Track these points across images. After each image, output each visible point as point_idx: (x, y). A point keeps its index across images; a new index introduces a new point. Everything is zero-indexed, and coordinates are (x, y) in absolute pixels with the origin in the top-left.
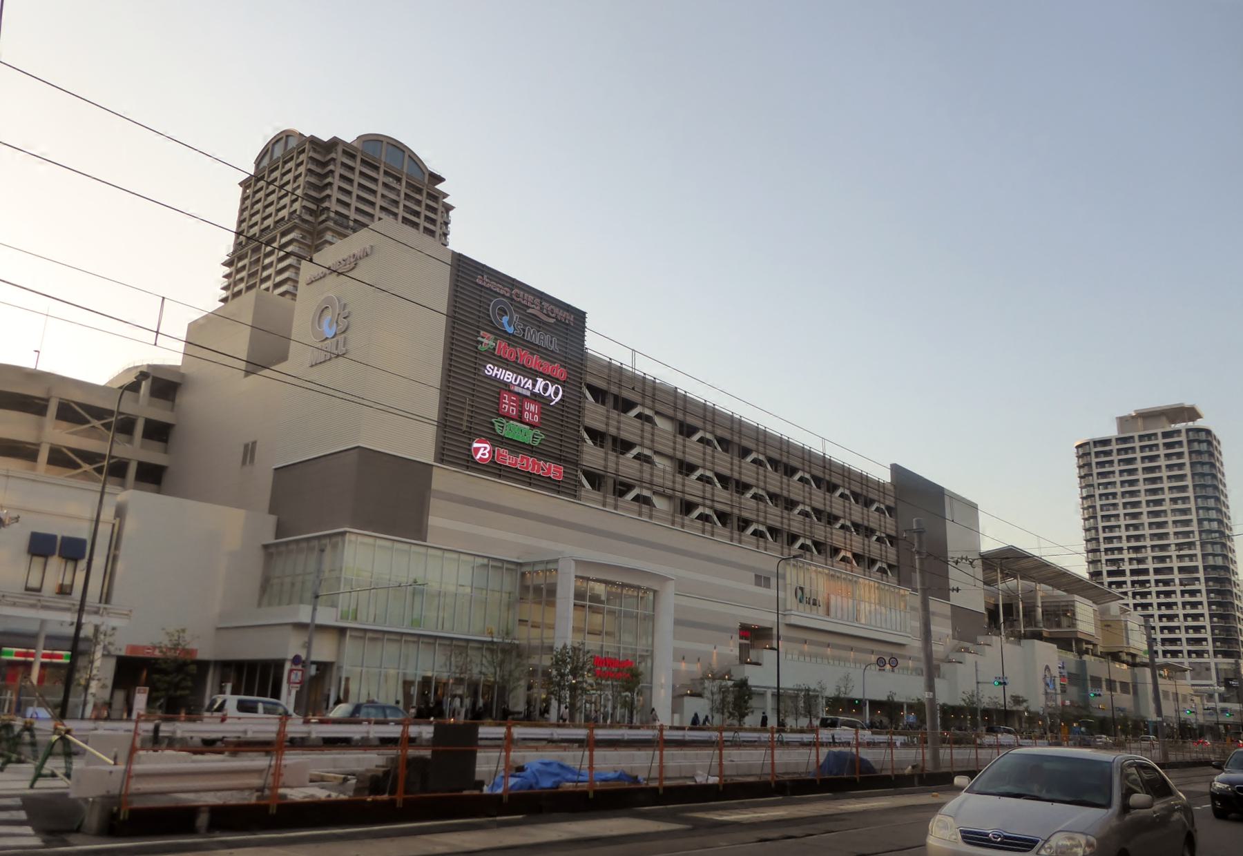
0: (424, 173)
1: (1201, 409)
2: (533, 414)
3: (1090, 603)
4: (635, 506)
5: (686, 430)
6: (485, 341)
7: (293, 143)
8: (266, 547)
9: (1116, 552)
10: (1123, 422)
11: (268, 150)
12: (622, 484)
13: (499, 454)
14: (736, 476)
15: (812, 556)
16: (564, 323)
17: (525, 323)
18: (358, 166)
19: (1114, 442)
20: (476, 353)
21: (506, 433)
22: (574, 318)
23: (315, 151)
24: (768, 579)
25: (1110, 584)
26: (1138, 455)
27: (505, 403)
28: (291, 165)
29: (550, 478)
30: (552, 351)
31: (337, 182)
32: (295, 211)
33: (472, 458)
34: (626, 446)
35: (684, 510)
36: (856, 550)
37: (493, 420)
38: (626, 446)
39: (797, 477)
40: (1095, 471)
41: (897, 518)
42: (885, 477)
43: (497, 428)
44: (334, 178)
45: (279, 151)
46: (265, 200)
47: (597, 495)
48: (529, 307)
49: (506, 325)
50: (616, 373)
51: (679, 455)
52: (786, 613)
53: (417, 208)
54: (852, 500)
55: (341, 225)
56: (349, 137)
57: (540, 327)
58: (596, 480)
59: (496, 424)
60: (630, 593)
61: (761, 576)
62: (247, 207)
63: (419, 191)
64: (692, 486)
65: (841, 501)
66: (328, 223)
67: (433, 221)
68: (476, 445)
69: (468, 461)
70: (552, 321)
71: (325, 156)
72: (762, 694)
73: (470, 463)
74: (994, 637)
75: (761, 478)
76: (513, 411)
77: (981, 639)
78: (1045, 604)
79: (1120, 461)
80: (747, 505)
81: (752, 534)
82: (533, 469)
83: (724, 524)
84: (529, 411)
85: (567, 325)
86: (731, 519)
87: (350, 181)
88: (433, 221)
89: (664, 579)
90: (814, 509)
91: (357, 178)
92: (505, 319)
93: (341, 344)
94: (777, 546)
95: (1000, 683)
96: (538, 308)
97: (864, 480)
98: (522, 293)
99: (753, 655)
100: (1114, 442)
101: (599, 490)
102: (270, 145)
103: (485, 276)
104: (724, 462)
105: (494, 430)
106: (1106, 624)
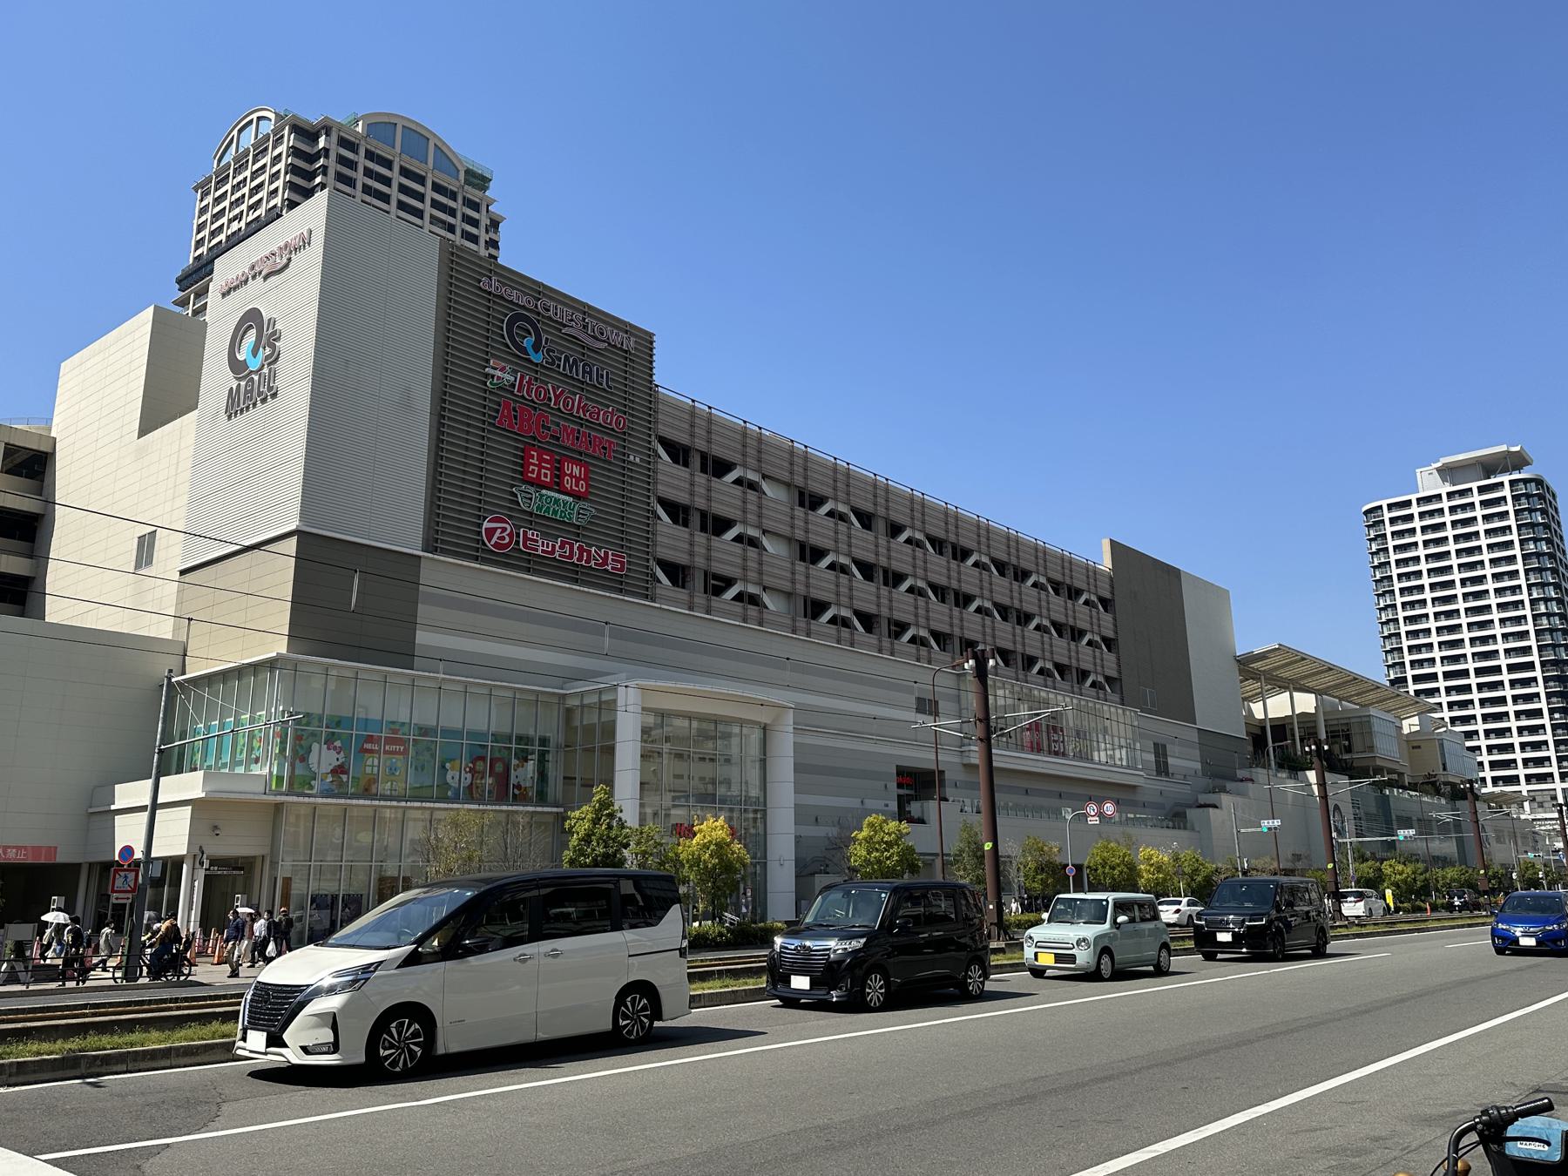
0: (458, 171)
1: (1531, 454)
2: (578, 480)
4: (738, 607)
9: (1423, 649)
12: (716, 577)
15: (1054, 682)
16: (621, 349)
25: (1417, 693)
26: (1448, 518)
27: (533, 464)
28: (267, 160)
29: (606, 570)
34: (720, 525)
36: (1059, 659)
38: (720, 525)
40: (1391, 543)
41: (1115, 613)
48: (565, 326)
49: (530, 350)
52: (964, 749)
53: (450, 220)
54: (1100, 607)
58: (678, 574)
61: (925, 700)
63: (453, 196)
64: (820, 582)
65: (1086, 609)
69: (477, 550)
72: (931, 864)
74: (1260, 770)
77: (1241, 773)
80: (900, 603)
81: (1091, 686)
82: (580, 559)
84: (571, 475)
85: (626, 352)
86: (1070, 670)
99: (915, 808)
101: (683, 587)
102: (235, 132)
104: (865, 544)
105: (519, 504)
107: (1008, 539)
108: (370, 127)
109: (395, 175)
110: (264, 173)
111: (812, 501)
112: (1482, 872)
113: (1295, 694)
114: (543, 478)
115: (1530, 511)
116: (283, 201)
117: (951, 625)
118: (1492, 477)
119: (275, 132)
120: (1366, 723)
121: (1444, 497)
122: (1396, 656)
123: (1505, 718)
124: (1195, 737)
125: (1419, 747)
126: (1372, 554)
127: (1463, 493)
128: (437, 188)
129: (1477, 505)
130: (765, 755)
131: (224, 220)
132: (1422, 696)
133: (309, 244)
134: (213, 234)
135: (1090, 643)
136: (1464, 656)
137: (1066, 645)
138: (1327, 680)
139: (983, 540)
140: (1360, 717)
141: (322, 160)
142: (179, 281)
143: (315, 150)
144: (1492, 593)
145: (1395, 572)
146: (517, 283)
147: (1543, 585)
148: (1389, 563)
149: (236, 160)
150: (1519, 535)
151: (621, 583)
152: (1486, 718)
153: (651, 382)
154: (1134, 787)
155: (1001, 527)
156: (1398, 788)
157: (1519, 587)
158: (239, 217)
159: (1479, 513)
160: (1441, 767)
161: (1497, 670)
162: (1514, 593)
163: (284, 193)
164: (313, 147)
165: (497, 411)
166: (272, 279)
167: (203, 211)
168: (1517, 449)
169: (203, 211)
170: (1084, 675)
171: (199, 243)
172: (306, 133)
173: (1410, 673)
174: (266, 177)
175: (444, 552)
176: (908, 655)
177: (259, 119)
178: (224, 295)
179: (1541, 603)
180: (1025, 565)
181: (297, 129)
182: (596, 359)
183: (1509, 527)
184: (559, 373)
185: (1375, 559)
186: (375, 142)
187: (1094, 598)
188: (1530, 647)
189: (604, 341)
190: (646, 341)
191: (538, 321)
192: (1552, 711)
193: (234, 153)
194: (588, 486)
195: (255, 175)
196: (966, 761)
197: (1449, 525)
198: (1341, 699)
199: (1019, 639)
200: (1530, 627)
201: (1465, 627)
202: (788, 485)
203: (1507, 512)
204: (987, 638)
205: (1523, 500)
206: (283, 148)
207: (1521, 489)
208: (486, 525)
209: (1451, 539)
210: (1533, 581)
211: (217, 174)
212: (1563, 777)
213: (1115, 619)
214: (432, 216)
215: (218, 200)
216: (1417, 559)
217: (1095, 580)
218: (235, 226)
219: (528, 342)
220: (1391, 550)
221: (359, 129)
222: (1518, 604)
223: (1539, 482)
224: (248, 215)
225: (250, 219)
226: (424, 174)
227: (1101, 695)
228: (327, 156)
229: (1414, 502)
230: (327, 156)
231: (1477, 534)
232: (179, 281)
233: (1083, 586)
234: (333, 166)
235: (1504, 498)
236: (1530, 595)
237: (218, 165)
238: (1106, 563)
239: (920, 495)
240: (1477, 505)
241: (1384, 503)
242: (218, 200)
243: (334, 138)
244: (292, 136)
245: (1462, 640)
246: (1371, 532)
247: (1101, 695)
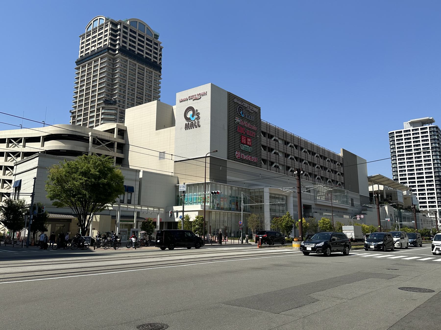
0: (152, 34)
1: (435, 119)
5: (286, 143)
6: (237, 120)
14: (268, 146)
15: (321, 181)
18: (129, 32)
25: (401, 183)
26: (412, 136)
28: (103, 31)
36: (310, 172)
39: (273, 139)
40: (396, 142)
48: (247, 108)
49: (242, 114)
50: (268, 126)
51: (285, 152)
52: (315, 200)
53: (151, 48)
58: (265, 161)
63: (151, 42)
67: (156, 54)
69: (235, 158)
78: (387, 193)
81: (290, 171)
82: (250, 160)
85: (256, 112)
86: (335, 181)
88: (156, 54)
90: (309, 162)
91: (129, 37)
97: (334, 155)
102: (92, 22)
104: (296, 152)
105: (240, 148)
107: (284, 133)
108: (130, 22)
109: (137, 36)
110: (102, 34)
111: (286, 143)
112: (416, 230)
113: (380, 185)
115: (434, 135)
116: (109, 43)
117: (267, 157)
118: (424, 125)
119: (105, 23)
120: (396, 193)
121: (411, 130)
122: (396, 173)
123: (424, 190)
124: (359, 197)
125: (406, 199)
126: (391, 145)
127: (416, 130)
128: (147, 39)
129: (420, 133)
130: (287, 202)
131: (90, 46)
132: (411, 187)
133: (206, 95)
134: (86, 50)
135: (305, 163)
136: (414, 173)
137: (298, 163)
138: (386, 183)
139: (277, 133)
140: (395, 192)
141: (119, 32)
142: (76, 62)
143: (117, 29)
144: (422, 157)
145: (397, 150)
146: (239, 99)
147: (436, 155)
148: (395, 148)
149: (93, 30)
150: (431, 142)
151: (256, 164)
152: (419, 190)
153: (260, 119)
154: (347, 209)
155: (273, 126)
156: (402, 209)
157: (430, 156)
158: (95, 46)
159: (420, 135)
160: (412, 204)
161: (423, 177)
162: (428, 157)
163: (109, 41)
164: (116, 28)
165: (237, 128)
166: (195, 101)
167: (83, 43)
168: (431, 118)
169: (83, 43)
170: (272, 163)
171: (82, 52)
172: (115, 24)
173: (399, 177)
174: (103, 35)
175: (251, 165)
176: (273, 170)
177: (100, 19)
178: (180, 102)
179: (436, 160)
180: (271, 133)
181: (112, 23)
182: (252, 115)
183: (428, 139)
184: (246, 119)
185: (391, 147)
186: (132, 27)
187: (306, 150)
188: (432, 172)
190: (259, 109)
192: (437, 189)
193: (92, 28)
194: (251, 143)
195: (99, 35)
196: (316, 203)
197: (412, 138)
198: (389, 187)
199: (285, 161)
200: (432, 166)
201: (415, 166)
202: (282, 140)
203: (428, 135)
204: (277, 161)
205: (432, 132)
206: (108, 28)
207: (432, 129)
208: (236, 153)
209: (412, 142)
210: (434, 154)
211: (87, 33)
212: (439, 206)
213: (343, 169)
214: (146, 47)
215: (87, 41)
216: (403, 147)
217: (293, 139)
218: (93, 48)
219: (241, 112)
220: (396, 144)
221: (128, 23)
222: (429, 160)
223: (437, 128)
224: (97, 46)
225: (98, 47)
226: (144, 35)
227: (320, 181)
228: (120, 31)
229: (403, 132)
230: (120, 31)
231: (419, 141)
232: (76, 62)
233: (290, 141)
234: (122, 34)
235: (427, 132)
236: (433, 158)
237: (87, 31)
238: (341, 154)
239: (269, 124)
240: (420, 133)
241: (395, 131)
242: (87, 41)
243: (122, 26)
244: (111, 25)
245: (414, 169)
246: (391, 139)
247: (320, 181)
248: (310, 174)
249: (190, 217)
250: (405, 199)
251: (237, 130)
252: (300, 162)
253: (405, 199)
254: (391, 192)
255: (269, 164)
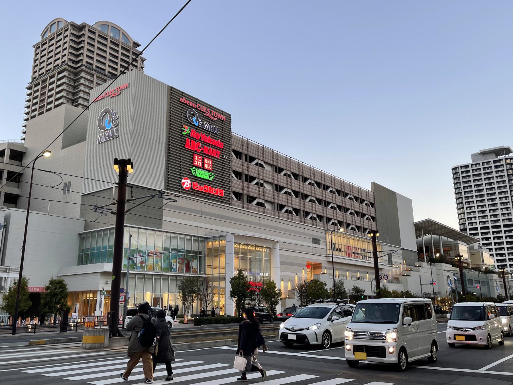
0: (130, 42)
2: (209, 165)
3: (465, 244)
7: (62, 25)
8: (80, 234)
10: (473, 156)
11: (48, 29)
12: (251, 197)
13: (194, 185)
15: (356, 233)
17: (203, 121)
18: (97, 38)
19: (470, 166)
20: (181, 136)
21: (198, 175)
22: (226, 118)
23: (74, 29)
24: (318, 240)
25: (471, 234)
26: (482, 172)
28: (61, 37)
30: (216, 134)
31: (86, 46)
32: (65, 61)
33: (182, 187)
34: (251, 179)
35: (279, 209)
37: (191, 169)
38: (251, 179)
40: (462, 180)
41: (375, 208)
42: (368, 187)
43: (193, 172)
44: (84, 44)
45: (54, 30)
46: (41, 53)
47: (240, 203)
48: (205, 113)
49: (195, 122)
52: (328, 256)
55: (89, 68)
56: (91, 22)
57: (210, 122)
58: (239, 196)
59: (192, 170)
60: (259, 249)
62: (38, 59)
63: (128, 51)
64: (282, 198)
66: (82, 67)
68: (183, 181)
69: (180, 189)
70: (216, 119)
71: (79, 33)
73: (181, 189)
75: (289, 183)
76: (200, 164)
79: (473, 175)
82: (210, 192)
83: (297, 214)
84: (207, 164)
85: (222, 121)
87: (93, 46)
89: (275, 242)
91: (96, 45)
92: (194, 119)
93: (115, 133)
94: (321, 224)
95: (431, 284)
96: (209, 113)
97: (359, 190)
98: (201, 106)
100: (470, 166)
101: (240, 200)
102: (49, 26)
103: (184, 98)
104: (296, 185)
105: (191, 173)
106: (472, 253)
111: (279, 170)
114: (199, 165)
153: (230, 131)
177: (58, 22)
189: (216, 118)
190: (229, 116)
191: (197, 111)
220: (462, 183)
240: (493, 167)
248: (358, 228)
249: (55, 278)
250: (472, 255)
251: (185, 145)
252: (345, 212)
253: (472, 255)
254: (450, 245)
255: (302, 215)
